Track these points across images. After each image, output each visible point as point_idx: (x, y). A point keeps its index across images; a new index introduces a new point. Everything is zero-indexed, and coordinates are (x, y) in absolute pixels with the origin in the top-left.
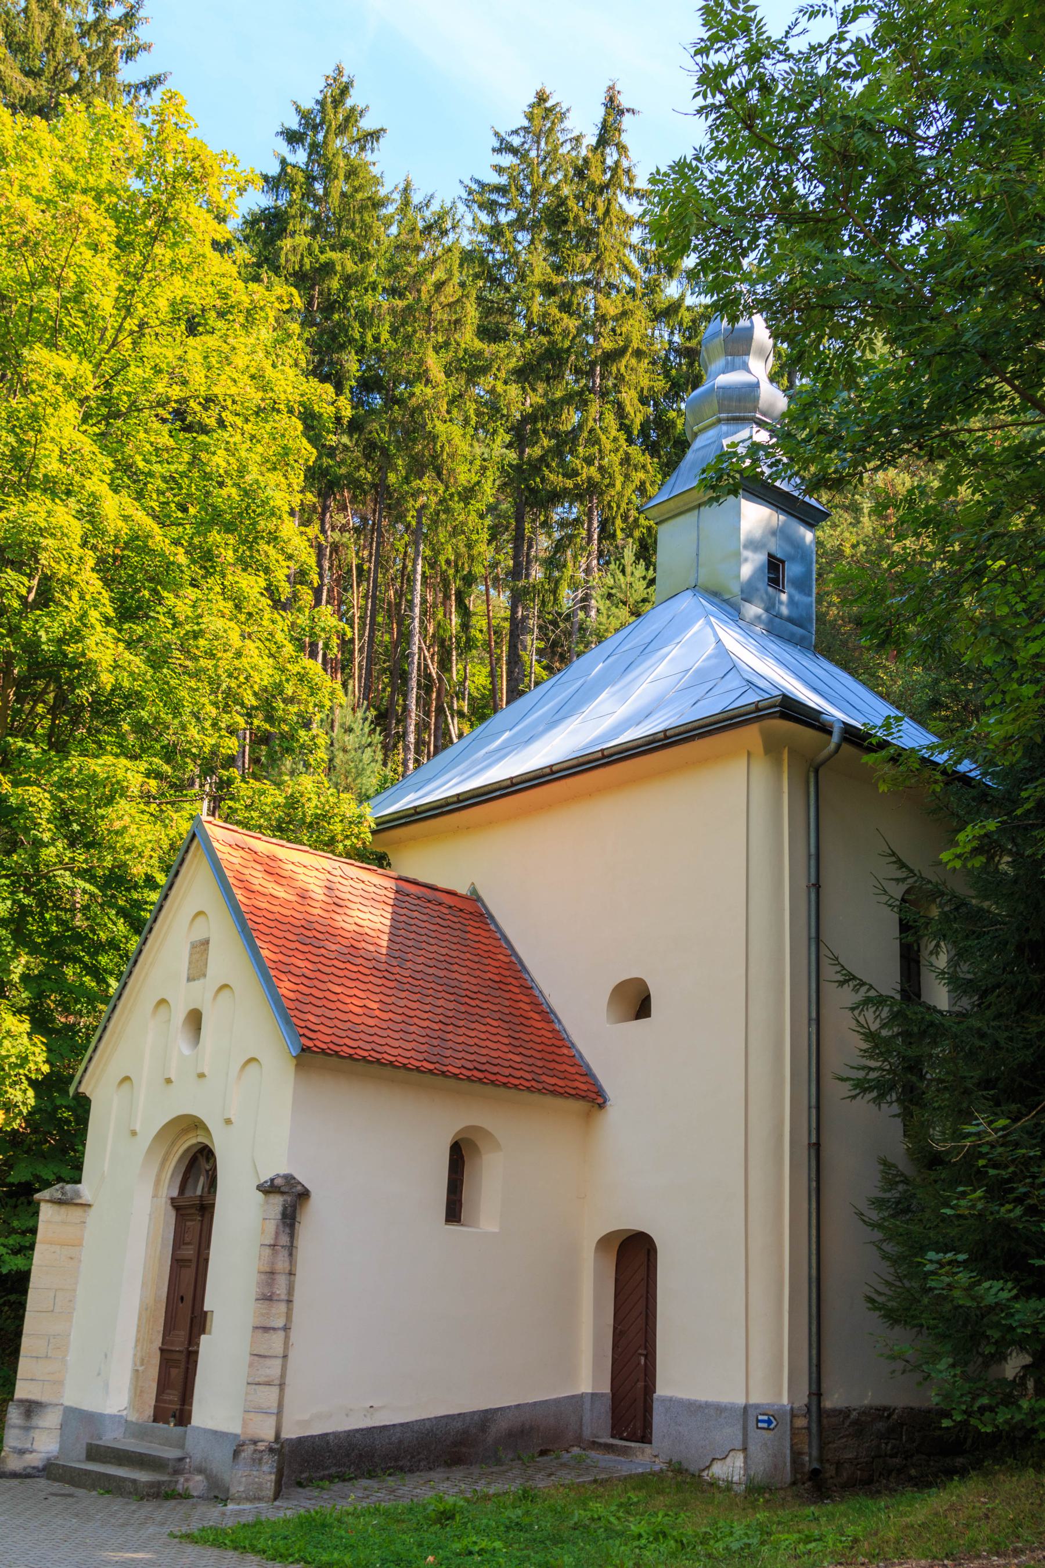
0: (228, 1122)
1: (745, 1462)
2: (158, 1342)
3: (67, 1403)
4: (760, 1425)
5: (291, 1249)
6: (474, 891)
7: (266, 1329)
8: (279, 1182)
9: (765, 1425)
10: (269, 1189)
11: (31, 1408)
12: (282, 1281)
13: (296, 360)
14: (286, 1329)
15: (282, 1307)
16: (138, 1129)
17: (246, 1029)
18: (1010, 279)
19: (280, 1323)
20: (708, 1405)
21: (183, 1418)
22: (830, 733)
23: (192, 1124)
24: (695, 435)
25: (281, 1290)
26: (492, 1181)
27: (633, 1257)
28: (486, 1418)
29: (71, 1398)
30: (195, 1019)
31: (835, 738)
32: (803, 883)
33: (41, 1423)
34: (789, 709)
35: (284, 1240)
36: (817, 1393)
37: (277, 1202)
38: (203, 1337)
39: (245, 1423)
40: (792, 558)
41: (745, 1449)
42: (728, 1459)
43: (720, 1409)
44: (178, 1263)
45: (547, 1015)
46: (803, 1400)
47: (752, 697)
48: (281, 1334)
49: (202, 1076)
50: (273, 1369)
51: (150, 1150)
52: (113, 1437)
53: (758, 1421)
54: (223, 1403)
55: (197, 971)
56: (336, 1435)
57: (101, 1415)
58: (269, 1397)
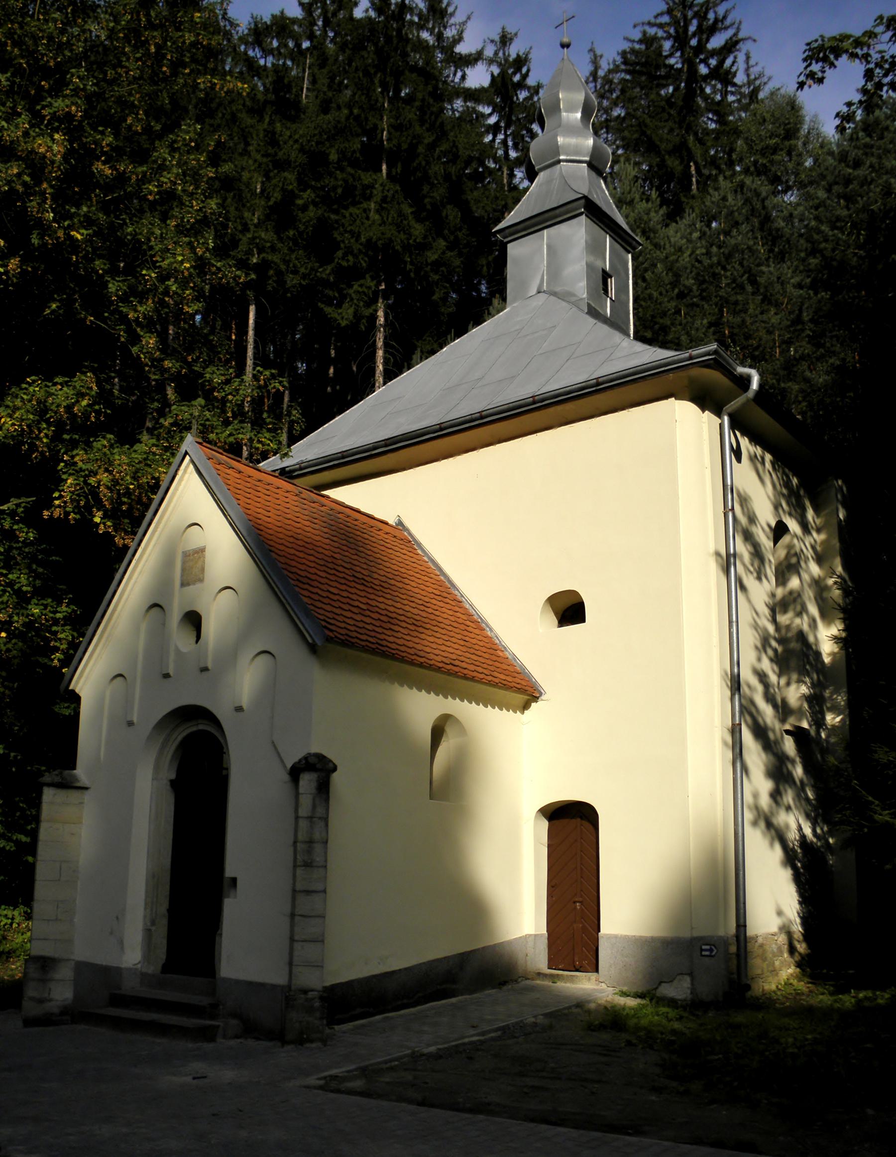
1: (692, 984)
3: (77, 959)
4: (704, 953)
6: (400, 523)
8: (312, 760)
9: (707, 953)
16: (135, 720)
18: (810, 50)
29: (82, 952)
33: (57, 976)
41: (691, 974)
42: (676, 982)
51: (149, 738)
52: (131, 986)
53: (702, 950)
54: (247, 950)
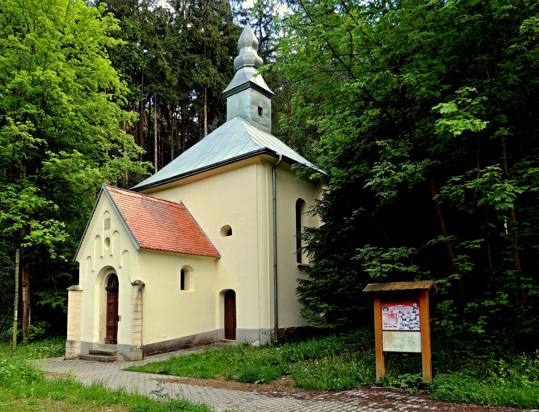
0: (120, 267)
2: (105, 324)
5: (142, 299)
6: (182, 203)
7: (137, 319)
10: (134, 284)
11: (72, 342)
12: (139, 307)
13: (348, 12)
14: (142, 319)
15: (140, 313)
17: (120, 242)
19: (140, 317)
20: (250, 330)
21: (115, 342)
22: (279, 158)
23: (111, 268)
24: (236, 71)
25: (140, 309)
26: (192, 279)
27: (229, 297)
28: (194, 337)
29: (83, 339)
30: (108, 240)
31: (280, 159)
32: (272, 199)
33: (75, 346)
34: (268, 151)
35: (140, 296)
36: (276, 325)
37: (136, 288)
38: (119, 322)
39: (133, 342)
40: (265, 107)
43: (253, 331)
44: (109, 304)
45: (204, 235)
46: (273, 326)
47: (257, 148)
48: (141, 320)
49: (111, 255)
50: (139, 329)
52: (96, 348)
55: (107, 227)
56: (156, 343)
57: (92, 343)
58: (139, 335)
